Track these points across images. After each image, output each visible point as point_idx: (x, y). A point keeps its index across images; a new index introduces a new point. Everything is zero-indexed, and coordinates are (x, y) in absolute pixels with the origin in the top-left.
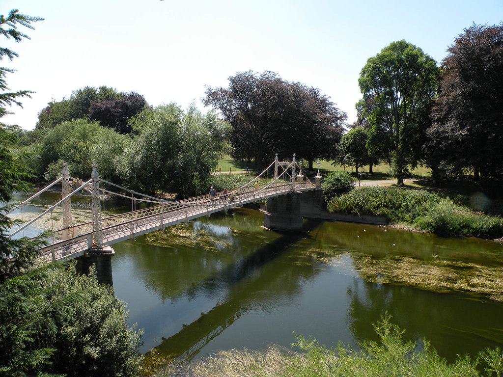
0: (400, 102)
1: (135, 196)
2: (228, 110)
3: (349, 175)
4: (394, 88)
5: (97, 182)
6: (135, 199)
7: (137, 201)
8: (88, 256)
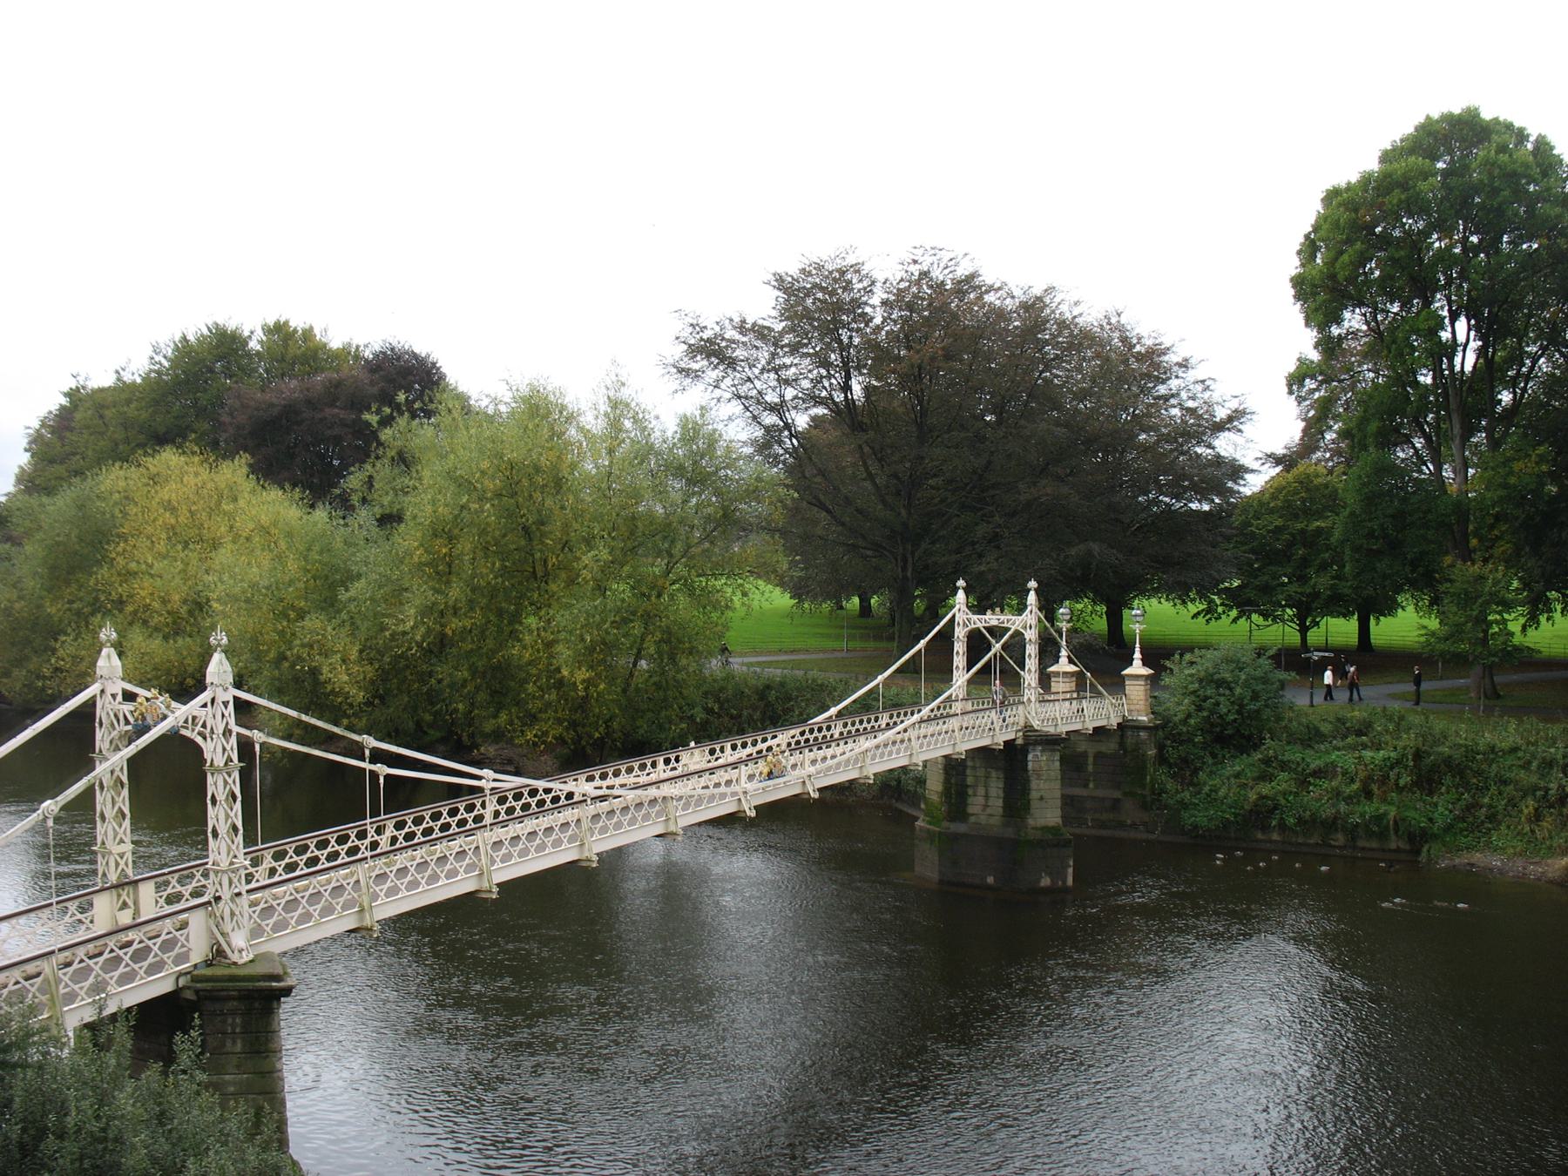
0: (1467, 361)
1: (378, 756)
2: (773, 408)
3: (1265, 663)
4: (1440, 304)
5: (226, 704)
6: (383, 770)
7: (387, 777)
8: (189, 995)
